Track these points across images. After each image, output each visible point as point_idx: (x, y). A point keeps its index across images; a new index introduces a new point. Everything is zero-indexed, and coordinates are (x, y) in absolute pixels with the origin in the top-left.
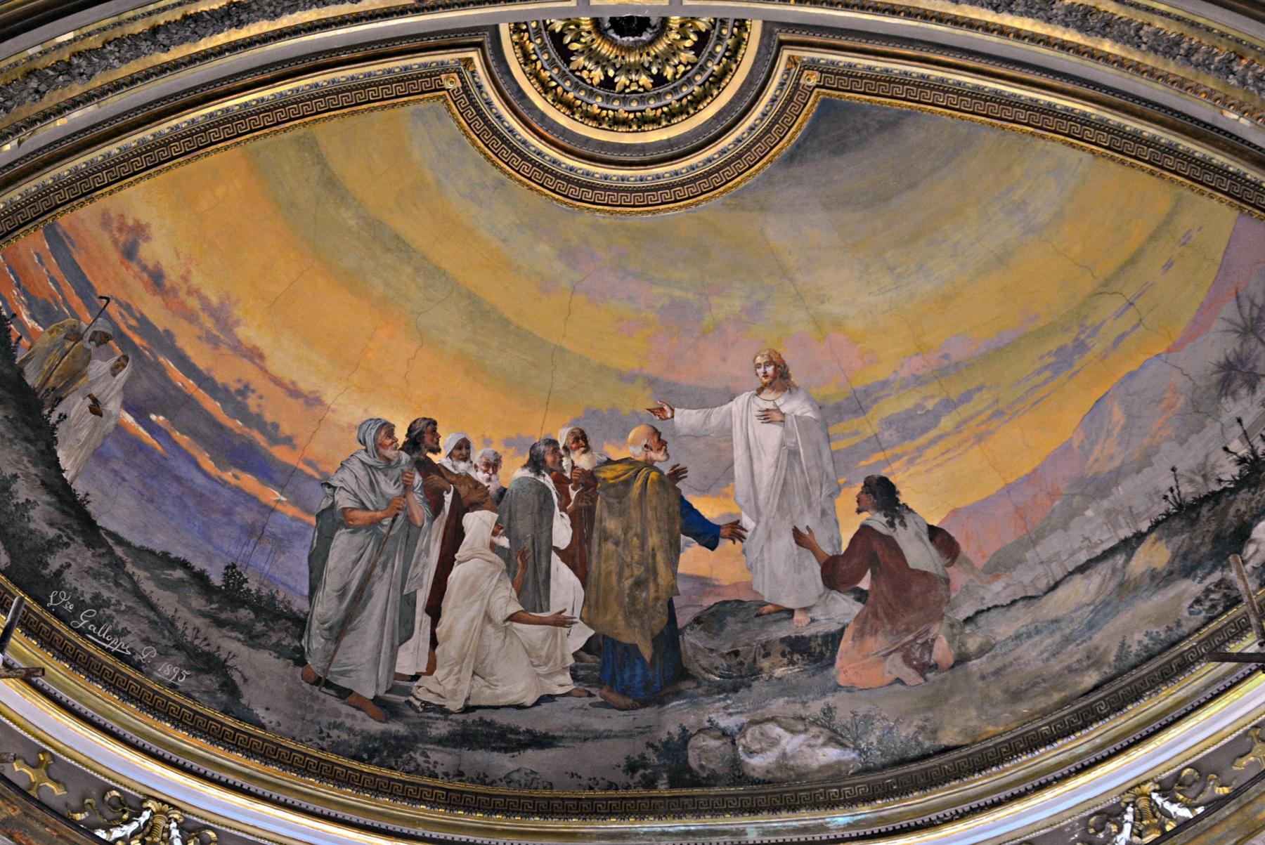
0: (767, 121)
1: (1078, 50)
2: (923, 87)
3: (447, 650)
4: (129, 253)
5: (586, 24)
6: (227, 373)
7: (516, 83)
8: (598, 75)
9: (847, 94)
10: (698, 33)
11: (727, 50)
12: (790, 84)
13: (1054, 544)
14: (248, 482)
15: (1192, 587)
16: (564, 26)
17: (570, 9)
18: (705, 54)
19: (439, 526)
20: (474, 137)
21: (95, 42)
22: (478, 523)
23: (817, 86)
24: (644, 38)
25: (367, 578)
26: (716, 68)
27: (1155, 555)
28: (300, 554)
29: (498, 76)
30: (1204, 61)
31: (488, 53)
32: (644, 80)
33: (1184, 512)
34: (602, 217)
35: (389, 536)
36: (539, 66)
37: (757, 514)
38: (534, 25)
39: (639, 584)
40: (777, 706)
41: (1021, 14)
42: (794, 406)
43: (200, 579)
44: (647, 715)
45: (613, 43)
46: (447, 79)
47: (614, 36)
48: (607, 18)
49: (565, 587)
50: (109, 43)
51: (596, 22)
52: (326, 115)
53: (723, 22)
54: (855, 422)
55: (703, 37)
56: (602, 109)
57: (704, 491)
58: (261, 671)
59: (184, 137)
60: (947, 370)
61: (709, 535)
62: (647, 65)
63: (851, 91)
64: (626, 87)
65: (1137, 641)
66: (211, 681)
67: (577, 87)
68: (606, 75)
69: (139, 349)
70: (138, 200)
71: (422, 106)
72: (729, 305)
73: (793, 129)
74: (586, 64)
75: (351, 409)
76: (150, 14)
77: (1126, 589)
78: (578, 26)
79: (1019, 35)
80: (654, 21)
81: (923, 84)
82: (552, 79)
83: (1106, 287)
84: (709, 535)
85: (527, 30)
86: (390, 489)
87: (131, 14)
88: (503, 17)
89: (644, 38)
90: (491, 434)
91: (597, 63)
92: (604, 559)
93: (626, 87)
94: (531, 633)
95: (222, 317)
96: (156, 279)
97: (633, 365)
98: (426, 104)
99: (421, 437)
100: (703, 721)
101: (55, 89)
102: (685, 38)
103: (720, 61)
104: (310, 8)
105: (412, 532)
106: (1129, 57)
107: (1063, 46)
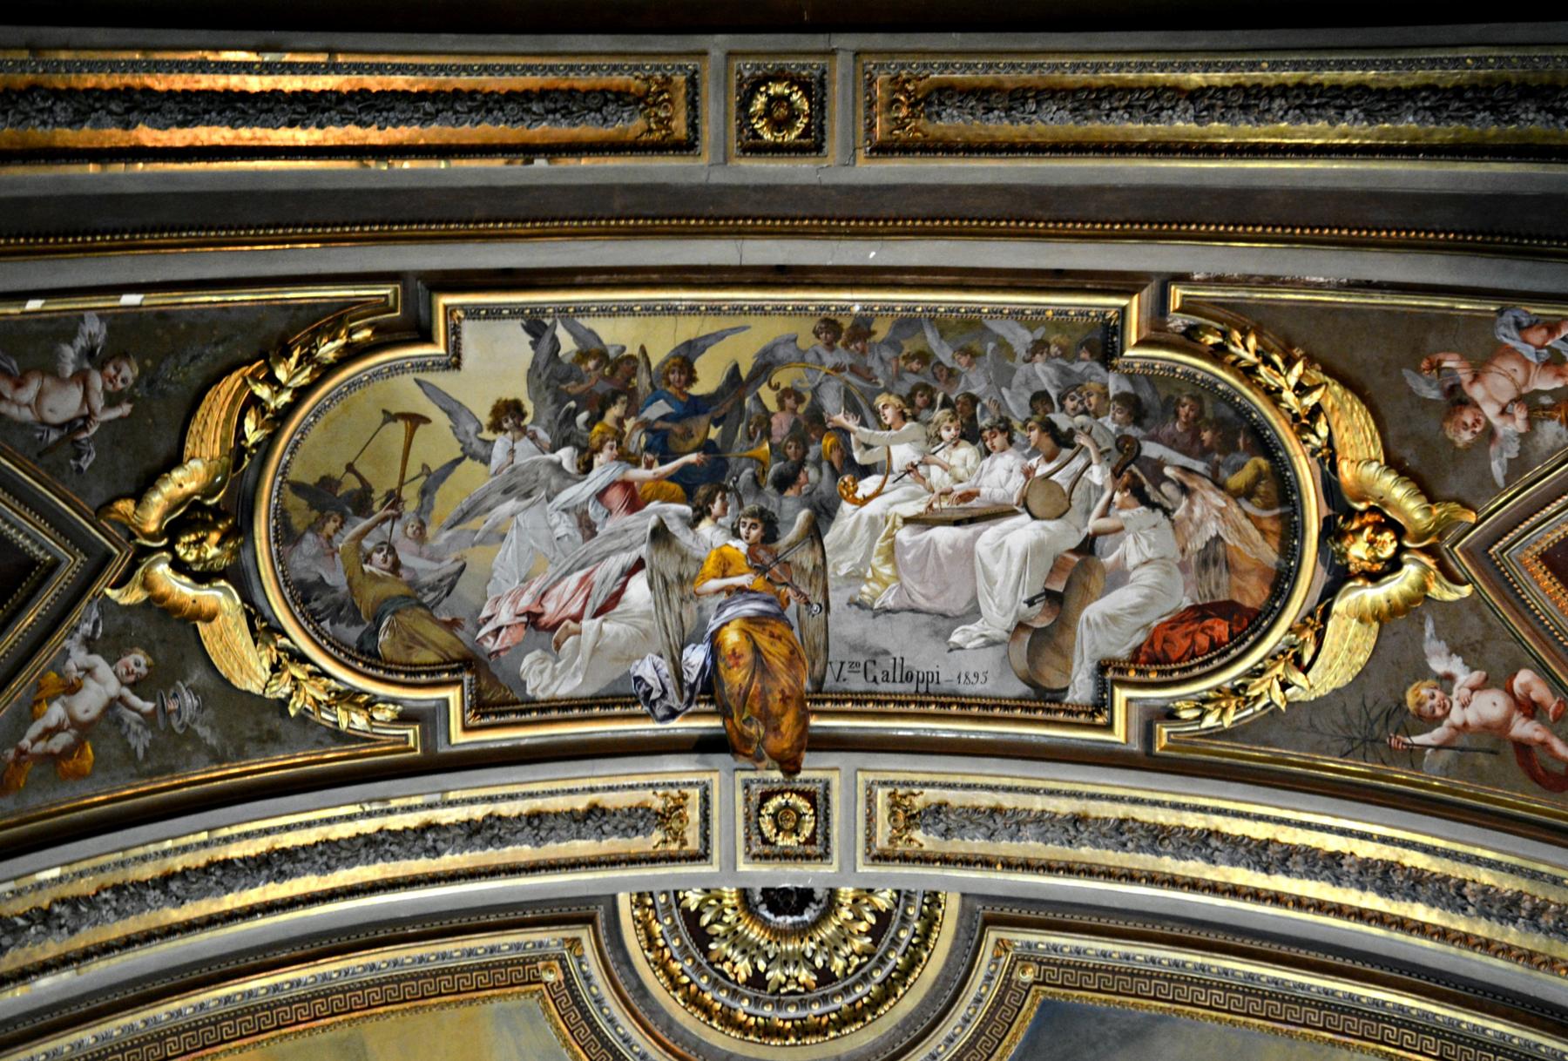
0: (970, 1030)
1: (1380, 919)
2: (1178, 981)
5: (730, 897)
7: (637, 976)
8: (743, 969)
9: (1076, 993)
10: (877, 913)
11: (914, 935)
12: (998, 980)
16: (702, 902)
17: (711, 876)
18: (886, 941)
20: (577, 1048)
21: (86, 886)
23: (1036, 983)
24: (806, 917)
26: (900, 961)
29: (612, 966)
30: (1556, 925)
31: (602, 933)
32: (804, 975)
36: (667, 953)
38: (662, 899)
41: (1301, 876)
45: (765, 924)
46: (545, 968)
47: (767, 914)
48: (758, 889)
50: (106, 890)
51: (744, 895)
52: (381, 1010)
53: (909, 897)
55: (883, 918)
56: (749, 1015)
59: (185, 1031)
62: (809, 954)
63: (1081, 988)
64: (781, 985)
67: (715, 984)
68: (755, 970)
71: (512, 1003)
73: (1005, 1042)
74: (729, 952)
76: (165, 854)
78: (719, 900)
79: (1299, 903)
80: (819, 894)
81: (1176, 979)
82: (684, 973)
85: (653, 907)
87: (140, 851)
88: (624, 884)
89: (806, 917)
91: (744, 952)
93: (781, 985)
98: (516, 1002)
101: (22, 946)
102: (859, 918)
103: (906, 951)
104: (375, 862)
106: (1453, 926)
107: (1360, 915)
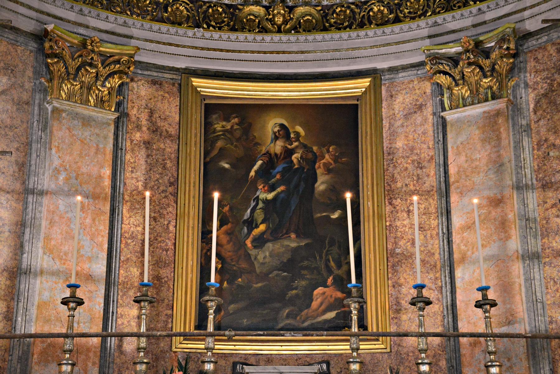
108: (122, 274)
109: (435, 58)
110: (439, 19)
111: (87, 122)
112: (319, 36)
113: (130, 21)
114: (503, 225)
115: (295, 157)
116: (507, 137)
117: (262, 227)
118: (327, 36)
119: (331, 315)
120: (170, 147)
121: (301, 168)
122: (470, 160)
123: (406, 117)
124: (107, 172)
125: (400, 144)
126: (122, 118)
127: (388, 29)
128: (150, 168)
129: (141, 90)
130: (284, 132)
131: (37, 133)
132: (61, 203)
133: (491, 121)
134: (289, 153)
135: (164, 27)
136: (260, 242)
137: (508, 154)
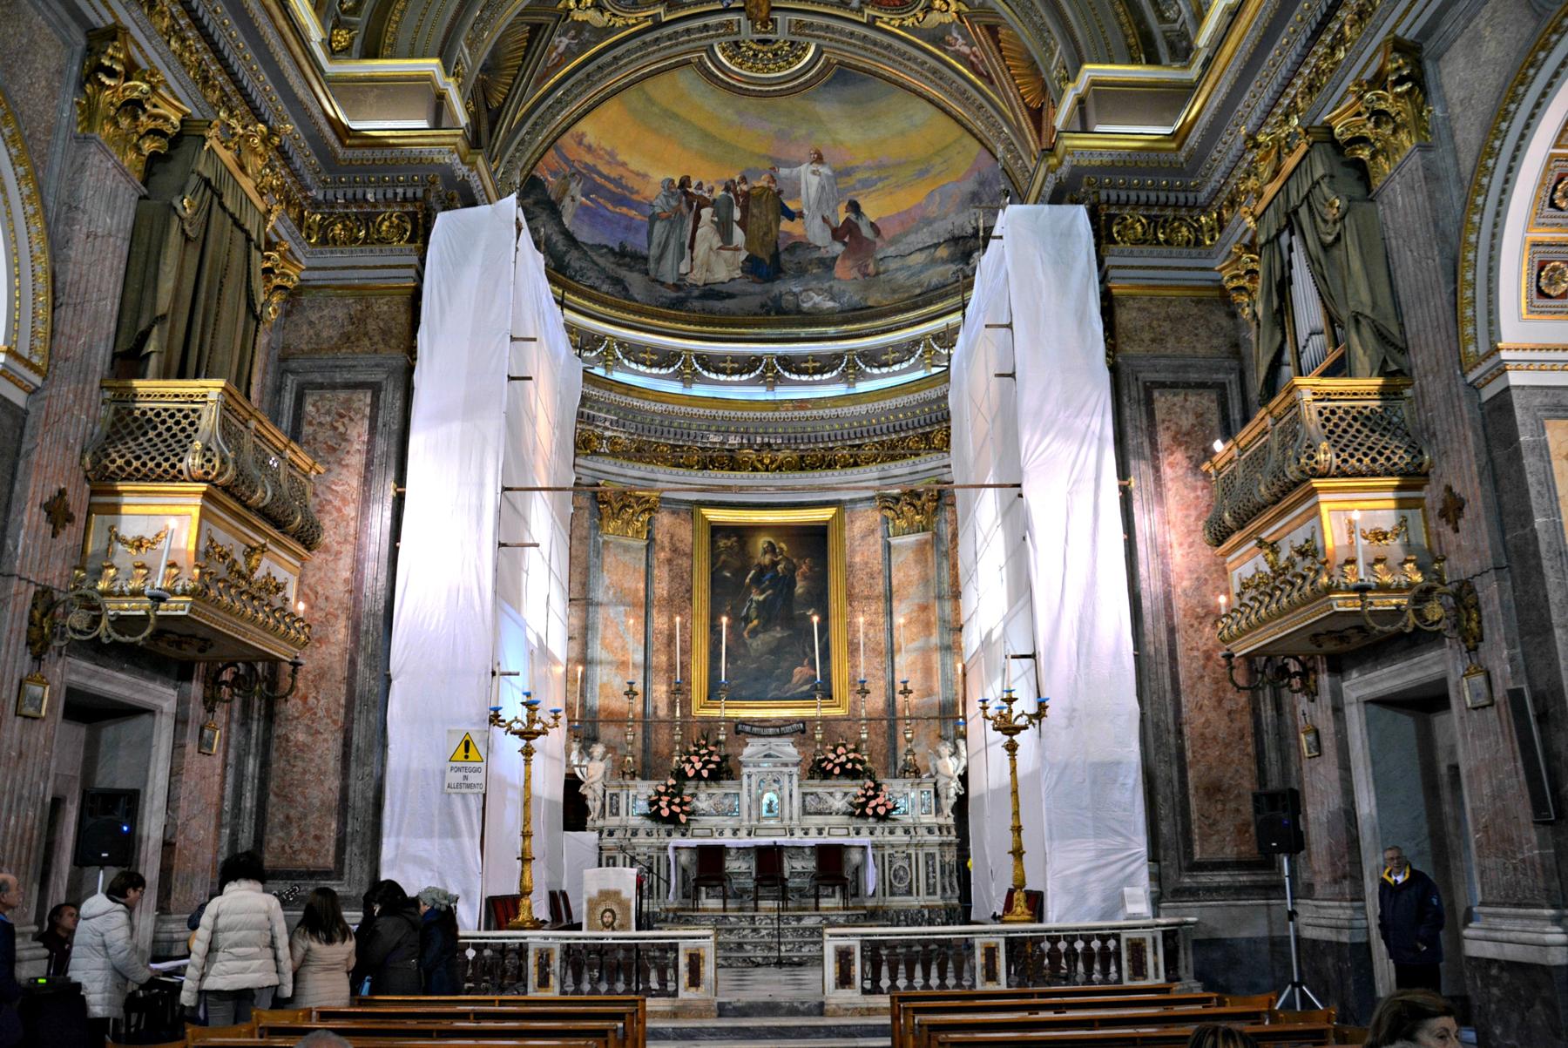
3: (697, 262)
4: (580, 143)
6: (614, 173)
13: (912, 238)
14: (624, 210)
15: (954, 267)
19: (692, 215)
22: (706, 213)
25: (668, 238)
27: (943, 252)
28: (644, 231)
33: (955, 240)
34: (752, 100)
35: (674, 220)
37: (809, 208)
39: (765, 234)
40: (814, 284)
42: (824, 170)
43: (611, 250)
44: (768, 286)
49: (738, 236)
54: (847, 179)
57: (790, 199)
58: (634, 280)
60: (881, 167)
61: (791, 216)
65: (935, 281)
66: (619, 288)
69: (585, 175)
70: (582, 126)
72: (802, 131)
75: (658, 176)
77: (934, 262)
83: (937, 153)
84: (791, 216)
86: (674, 203)
90: (710, 178)
92: (753, 225)
94: (727, 254)
95: (612, 154)
96: (589, 148)
97: (763, 151)
99: (685, 182)
100: (788, 287)
105: (682, 217)
108: (654, 660)
109: (883, 497)
110: (886, 466)
111: (627, 549)
112: (798, 474)
113: (656, 468)
114: (927, 626)
115: (780, 567)
116: (932, 558)
117: (755, 622)
118: (804, 474)
119: (807, 687)
120: (685, 562)
121: (784, 576)
122: (907, 575)
123: (863, 538)
124: (642, 585)
125: (858, 559)
126: (651, 539)
127: (849, 470)
128: (672, 579)
129: (664, 520)
130: (771, 548)
131: (593, 560)
132: (612, 611)
133: (921, 548)
134: (775, 564)
135: (681, 471)
136: (754, 633)
137: (932, 573)
